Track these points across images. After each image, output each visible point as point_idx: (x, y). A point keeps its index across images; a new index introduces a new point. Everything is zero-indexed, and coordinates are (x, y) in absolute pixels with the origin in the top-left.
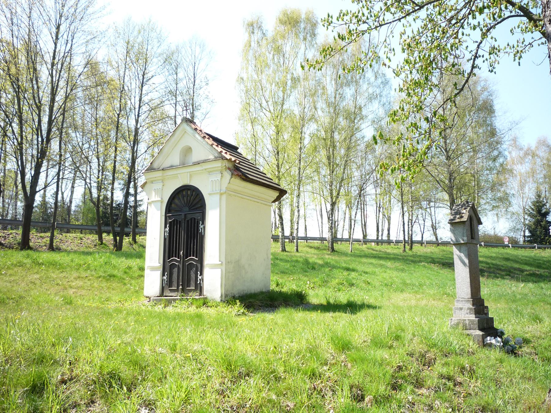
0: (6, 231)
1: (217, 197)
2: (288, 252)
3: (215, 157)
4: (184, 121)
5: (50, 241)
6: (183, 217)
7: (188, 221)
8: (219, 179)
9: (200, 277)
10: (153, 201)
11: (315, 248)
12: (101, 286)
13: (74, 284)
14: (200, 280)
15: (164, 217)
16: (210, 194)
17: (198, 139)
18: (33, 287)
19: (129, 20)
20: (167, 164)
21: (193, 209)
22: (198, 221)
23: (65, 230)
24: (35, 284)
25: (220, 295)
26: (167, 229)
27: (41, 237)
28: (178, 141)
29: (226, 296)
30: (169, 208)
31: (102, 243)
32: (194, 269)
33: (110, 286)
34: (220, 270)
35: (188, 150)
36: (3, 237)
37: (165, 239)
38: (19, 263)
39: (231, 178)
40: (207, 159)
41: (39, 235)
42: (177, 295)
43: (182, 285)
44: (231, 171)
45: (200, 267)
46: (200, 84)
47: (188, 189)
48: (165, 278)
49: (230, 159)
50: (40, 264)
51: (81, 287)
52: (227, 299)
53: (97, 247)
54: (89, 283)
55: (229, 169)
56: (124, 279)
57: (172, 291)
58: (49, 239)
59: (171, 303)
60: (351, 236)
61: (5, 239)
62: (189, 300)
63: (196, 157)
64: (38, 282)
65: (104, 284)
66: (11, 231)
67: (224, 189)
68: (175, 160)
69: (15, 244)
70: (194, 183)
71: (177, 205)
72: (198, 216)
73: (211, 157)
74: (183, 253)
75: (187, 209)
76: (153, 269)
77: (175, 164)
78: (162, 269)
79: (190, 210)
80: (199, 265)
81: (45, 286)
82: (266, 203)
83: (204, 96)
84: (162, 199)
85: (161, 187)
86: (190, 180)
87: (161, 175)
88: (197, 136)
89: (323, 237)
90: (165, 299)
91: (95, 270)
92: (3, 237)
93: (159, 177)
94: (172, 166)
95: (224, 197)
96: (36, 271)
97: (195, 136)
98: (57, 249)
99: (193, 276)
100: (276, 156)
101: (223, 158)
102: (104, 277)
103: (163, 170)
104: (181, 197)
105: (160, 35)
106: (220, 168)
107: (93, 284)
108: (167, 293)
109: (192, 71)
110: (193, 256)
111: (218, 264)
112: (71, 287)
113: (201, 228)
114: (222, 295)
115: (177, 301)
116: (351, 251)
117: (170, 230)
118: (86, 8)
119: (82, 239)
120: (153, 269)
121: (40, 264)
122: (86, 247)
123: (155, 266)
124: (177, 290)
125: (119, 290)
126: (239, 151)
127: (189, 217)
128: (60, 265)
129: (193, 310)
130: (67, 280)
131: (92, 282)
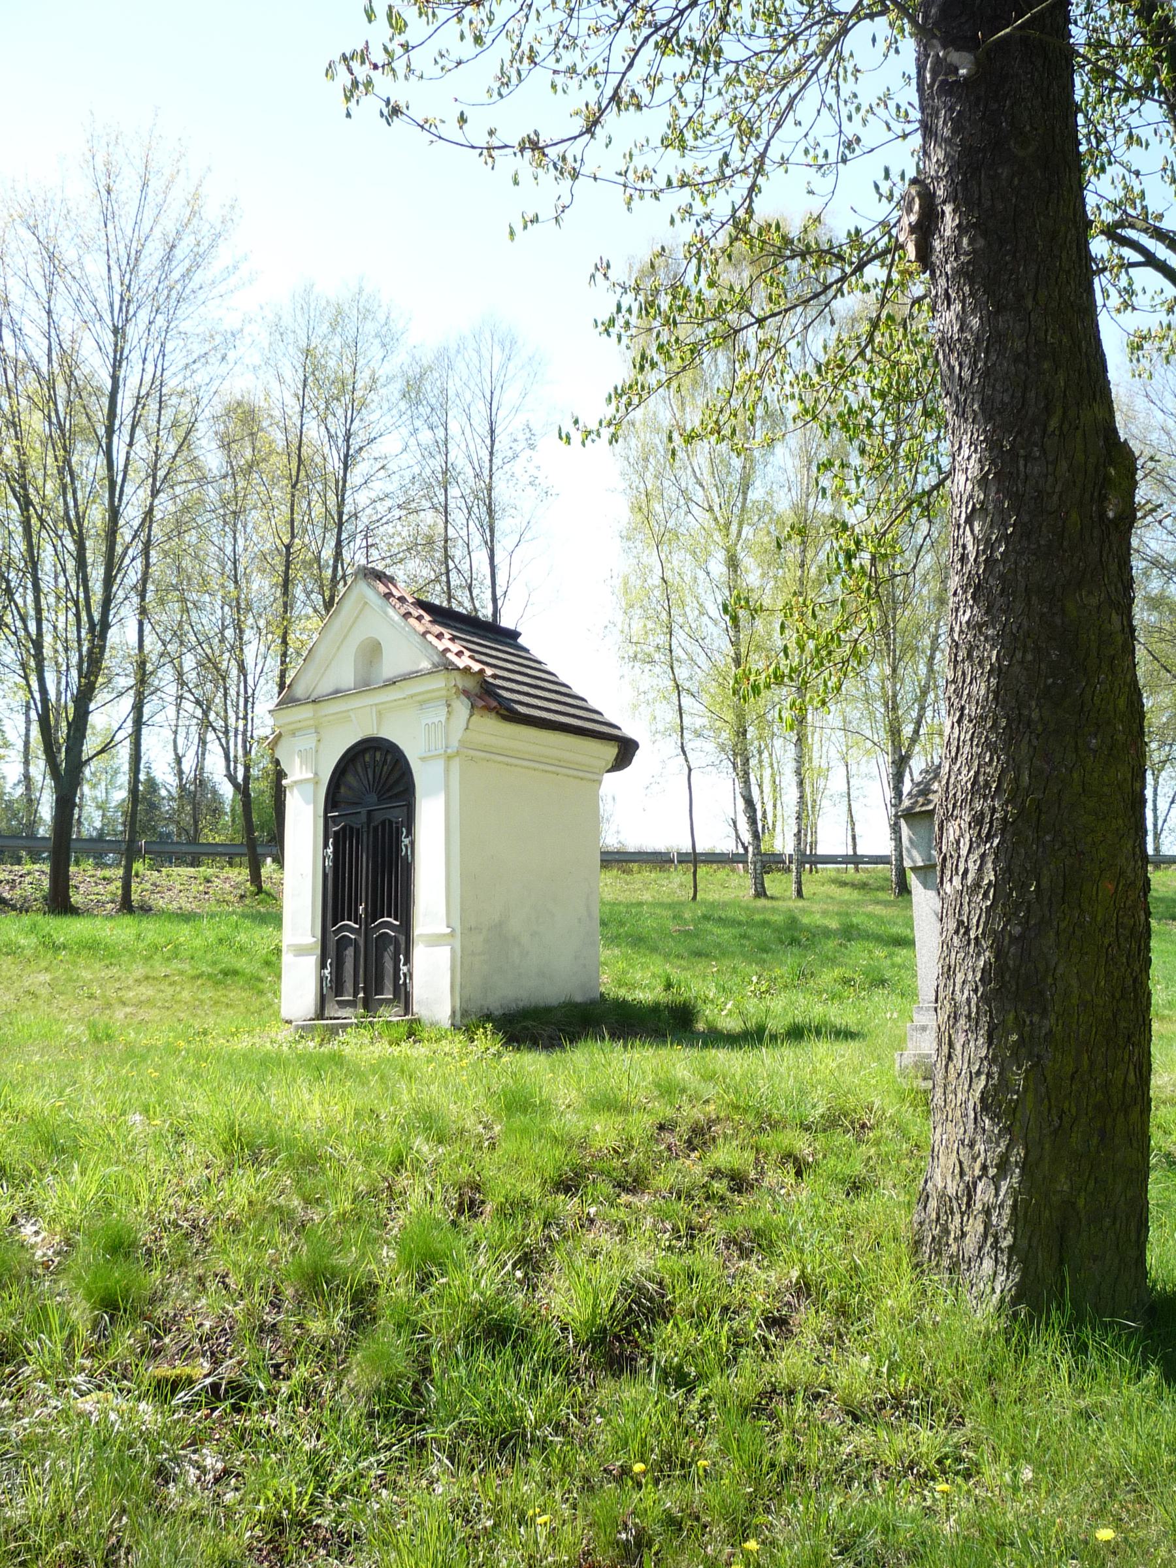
0: (16, 867)
1: (438, 767)
2: (772, 898)
3: (435, 666)
4: (360, 576)
5: (123, 888)
6: (364, 818)
7: (376, 829)
8: (443, 719)
9: (404, 969)
10: (295, 782)
11: (853, 885)
12: (198, 999)
13: (131, 994)
14: (405, 975)
15: (321, 821)
16: (423, 759)
18: (29, 1004)
19: (308, 291)
20: (325, 687)
21: (390, 797)
22: (397, 828)
23: (189, 859)
24: (36, 997)
25: (449, 1013)
26: (330, 850)
27: (104, 879)
28: (351, 627)
29: (465, 1013)
30: (333, 799)
31: (260, 890)
32: (392, 948)
33: (223, 999)
34: (449, 948)
35: (372, 651)
36: (8, 882)
38: (6, 946)
39: (471, 716)
40: (415, 669)
41: (100, 873)
42: (349, 1015)
43: (365, 990)
44: (468, 698)
45: (403, 945)
46: (514, 445)
47: (376, 749)
48: (327, 972)
49: (467, 669)
50: (57, 948)
51: (149, 1002)
52: (465, 1021)
53: (247, 902)
54: (170, 991)
55: (465, 692)
56: (261, 980)
57: (342, 1003)
58: (119, 884)
59: (338, 1034)
61: (12, 888)
62: (376, 1027)
63: (390, 666)
64: (44, 992)
65: (209, 994)
66: (29, 867)
67: (455, 744)
68: (344, 674)
69: (36, 900)
70: (390, 732)
71: (350, 788)
72: (398, 816)
73: (425, 665)
74: (366, 909)
75: (374, 797)
76: (300, 951)
77: (344, 686)
78: (319, 952)
79: (380, 800)
80: (402, 939)
81: (61, 1001)
82: (581, 774)
83: (525, 479)
84: (316, 774)
85: (313, 745)
86: (379, 724)
87: (310, 715)
88: (391, 612)
89: (859, 853)
90: (323, 1025)
91: (192, 958)
92: (8, 882)
93: (305, 720)
94: (337, 692)
95: (456, 765)
96: (43, 964)
97: (386, 613)
98: (141, 908)
99: (389, 965)
100: (731, 633)
101: (449, 667)
102: (210, 976)
103: (314, 701)
104: (360, 770)
105: (385, 328)
106: (444, 693)
107: (180, 993)
108: (332, 1010)
109: (485, 412)
110: (389, 916)
111: (444, 935)
112: (124, 1004)
113: (406, 846)
114: (454, 1013)
115: (349, 1030)
117: (335, 852)
118: (187, 275)
119: (209, 881)
120: (300, 951)
121: (57, 948)
122: (218, 901)
124: (352, 1004)
125: (242, 1009)
126: (520, 640)
127: (378, 817)
128: (106, 948)
129: (382, 1049)
130: (117, 985)
131: (178, 988)
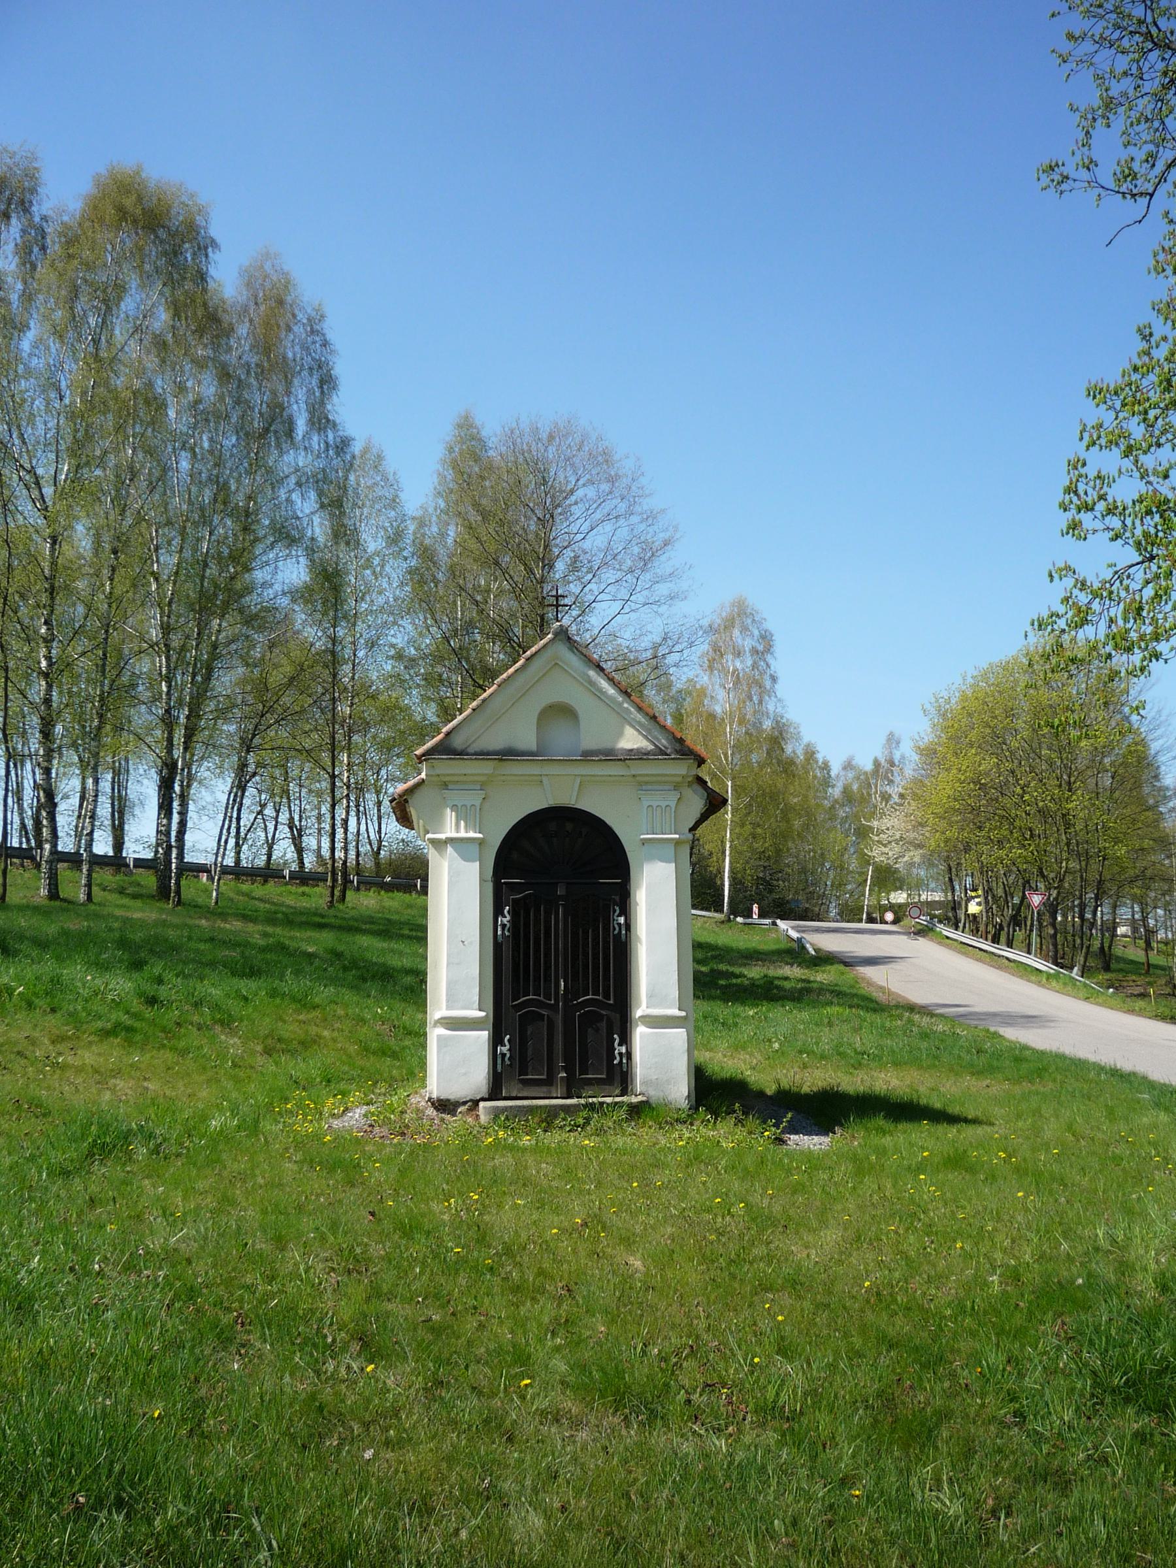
8: (673, 805)
15: (490, 887)
17: (605, 693)
20: (496, 740)
26: (506, 919)
37: (497, 946)
60: (220, 859)
85: (478, 803)
106: (680, 779)
111: (678, 1017)
116: (217, 903)
117: (514, 921)
123: (1035, 1031)
